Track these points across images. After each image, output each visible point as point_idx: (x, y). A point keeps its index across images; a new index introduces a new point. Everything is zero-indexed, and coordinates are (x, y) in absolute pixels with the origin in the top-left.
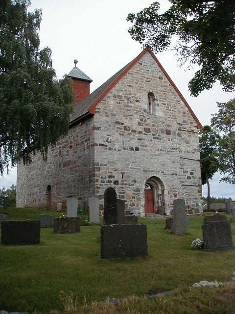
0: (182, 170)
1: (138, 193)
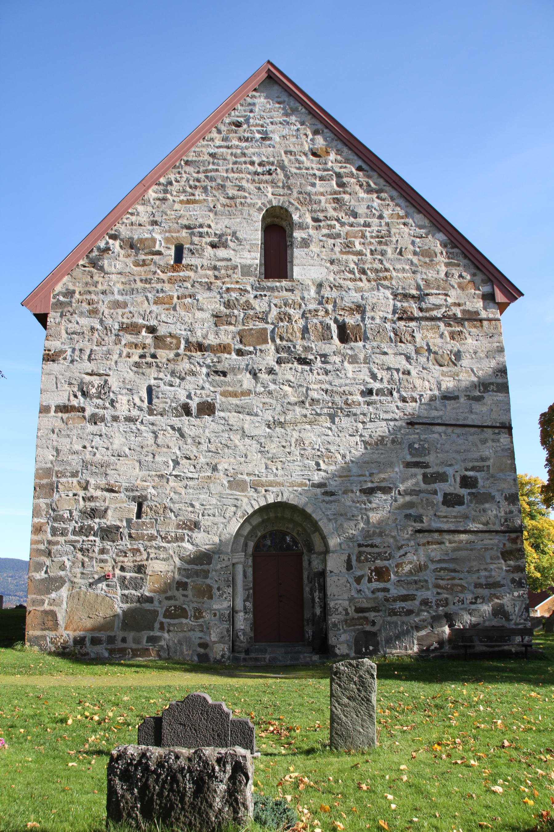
0: (419, 472)
1: (205, 567)
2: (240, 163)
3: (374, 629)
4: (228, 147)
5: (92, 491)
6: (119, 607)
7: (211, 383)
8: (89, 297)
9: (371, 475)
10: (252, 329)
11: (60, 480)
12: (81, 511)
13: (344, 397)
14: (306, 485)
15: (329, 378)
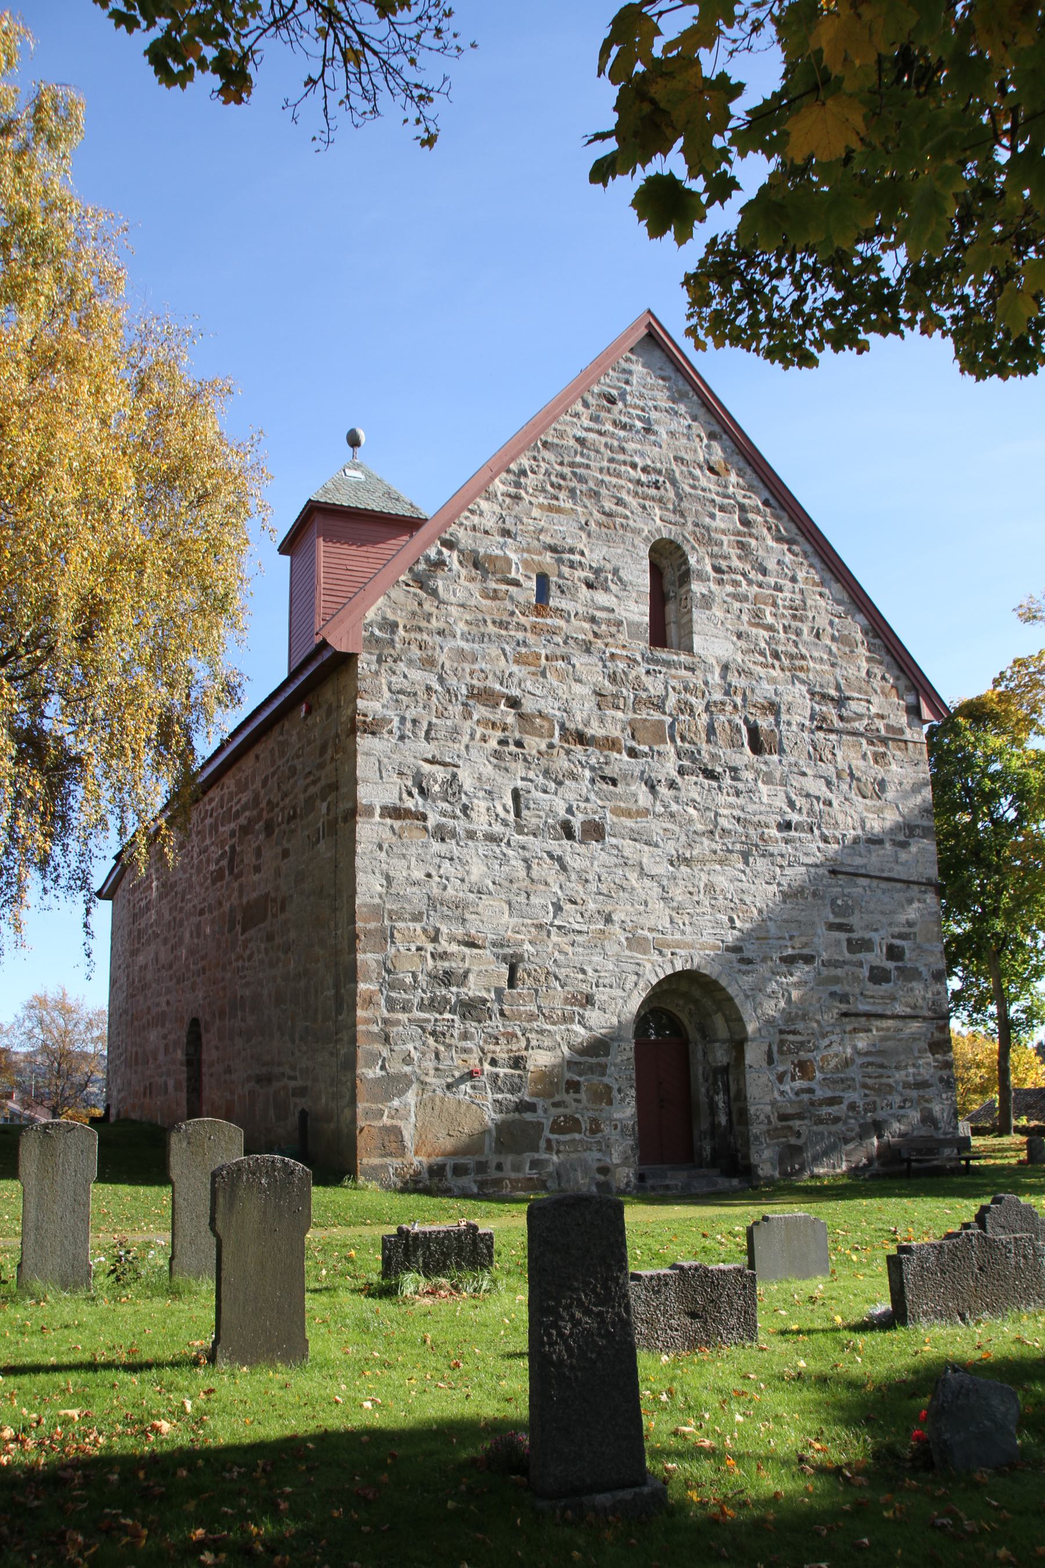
0: (843, 936)
1: (602, 1060)
2: (618, 462)
3: (800, 1142)
4: (600, 433)
5: (444, 945)
6: (490, 1116)
7: (597, 793)
8: (419, 636)
9: (791, 938)
10: (645, 720)
11: (396, 924)
12: (429, 975)
13: (760, 830)
14: (719, 948)
15: (740, 801)
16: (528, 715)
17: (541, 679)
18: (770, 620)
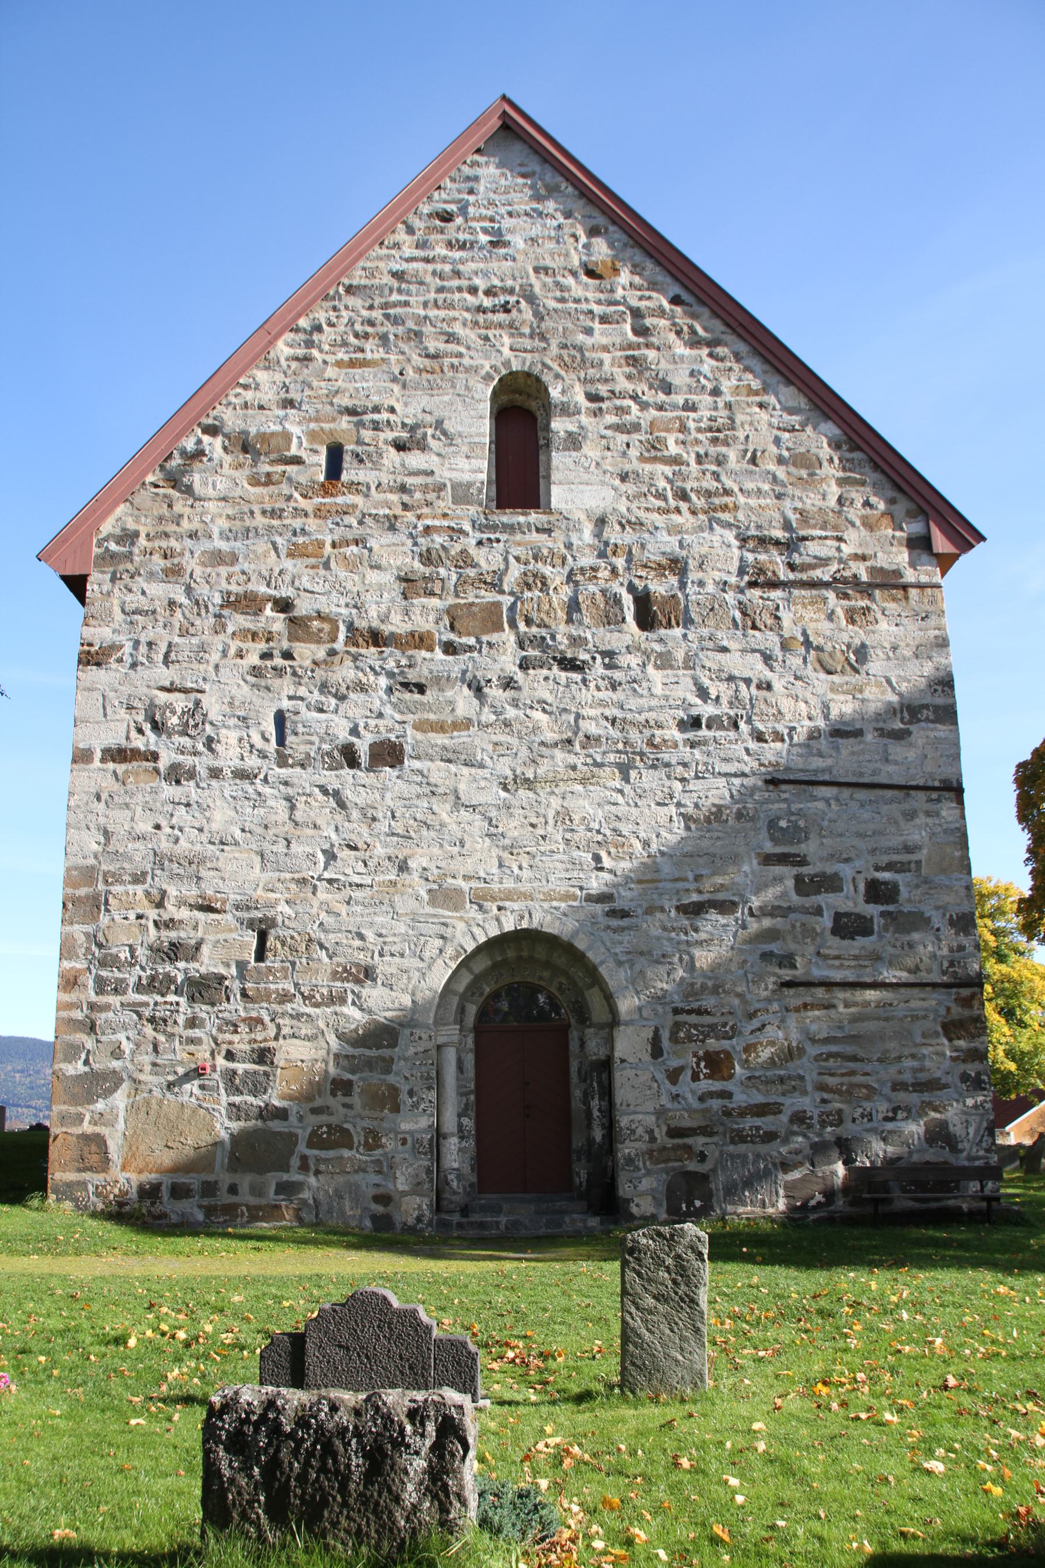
0: (788, 872)
1: (386, 1052)
2: (450, 290)
3: (702, 1168)
5: (171, 910)
6: (224, 1127)
7: (395, 706)
8: (164, 544)
9: (698, 878)
10: (472, 604)
11: (112, 888)
12: (151, 948)
13: (647, 733)
14: (574, 898)
15: (619, 696)
16: (302, 618)
17: (322, 572)
18: (673, 449)
